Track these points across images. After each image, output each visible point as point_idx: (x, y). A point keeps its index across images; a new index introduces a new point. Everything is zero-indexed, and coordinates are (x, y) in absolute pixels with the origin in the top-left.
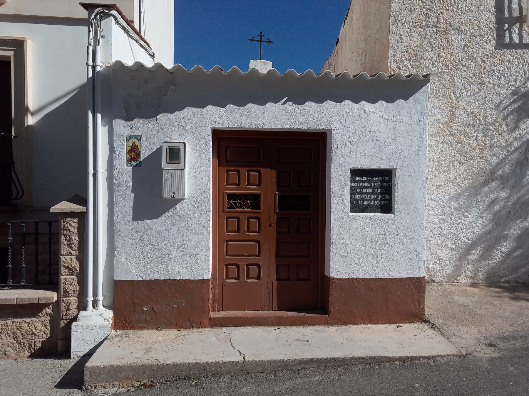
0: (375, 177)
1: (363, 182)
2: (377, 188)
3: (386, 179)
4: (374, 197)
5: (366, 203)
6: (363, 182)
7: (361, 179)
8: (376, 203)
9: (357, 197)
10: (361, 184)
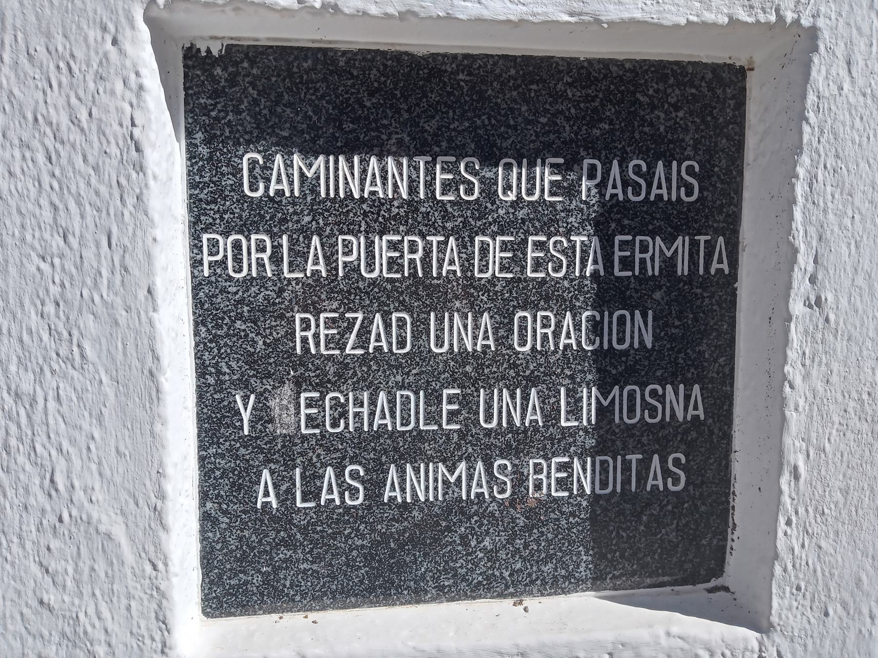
0: (529, 156)
1: (377, 216)
2: (545, 295)
3: (672, 182)
4: (506, 408)
5: (417, 485)
6: (377, 216)
7: (346, 176)
8: (545, 476)
9: (293, 411)
10: (352, 250)
